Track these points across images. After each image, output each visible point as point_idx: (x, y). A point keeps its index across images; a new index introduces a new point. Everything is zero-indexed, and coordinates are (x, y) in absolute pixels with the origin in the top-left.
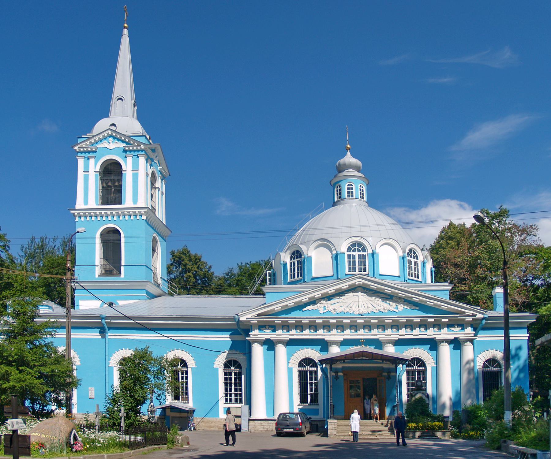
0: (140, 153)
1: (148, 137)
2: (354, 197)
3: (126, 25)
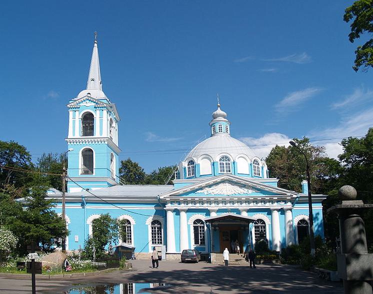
1: (108, 100)
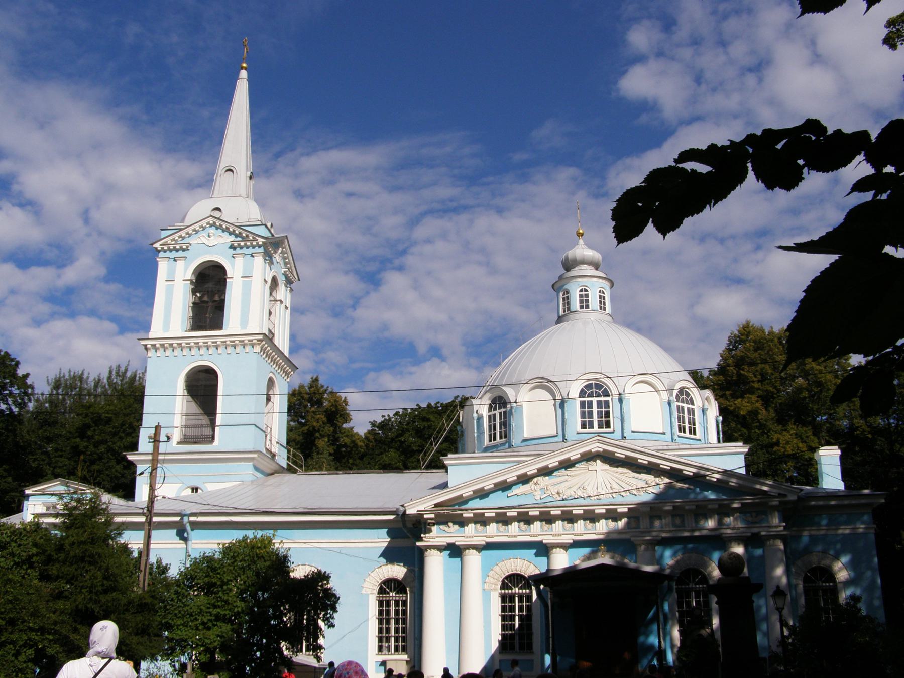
0: (257, 250)
1: (269, 225)
3: (244, 65)
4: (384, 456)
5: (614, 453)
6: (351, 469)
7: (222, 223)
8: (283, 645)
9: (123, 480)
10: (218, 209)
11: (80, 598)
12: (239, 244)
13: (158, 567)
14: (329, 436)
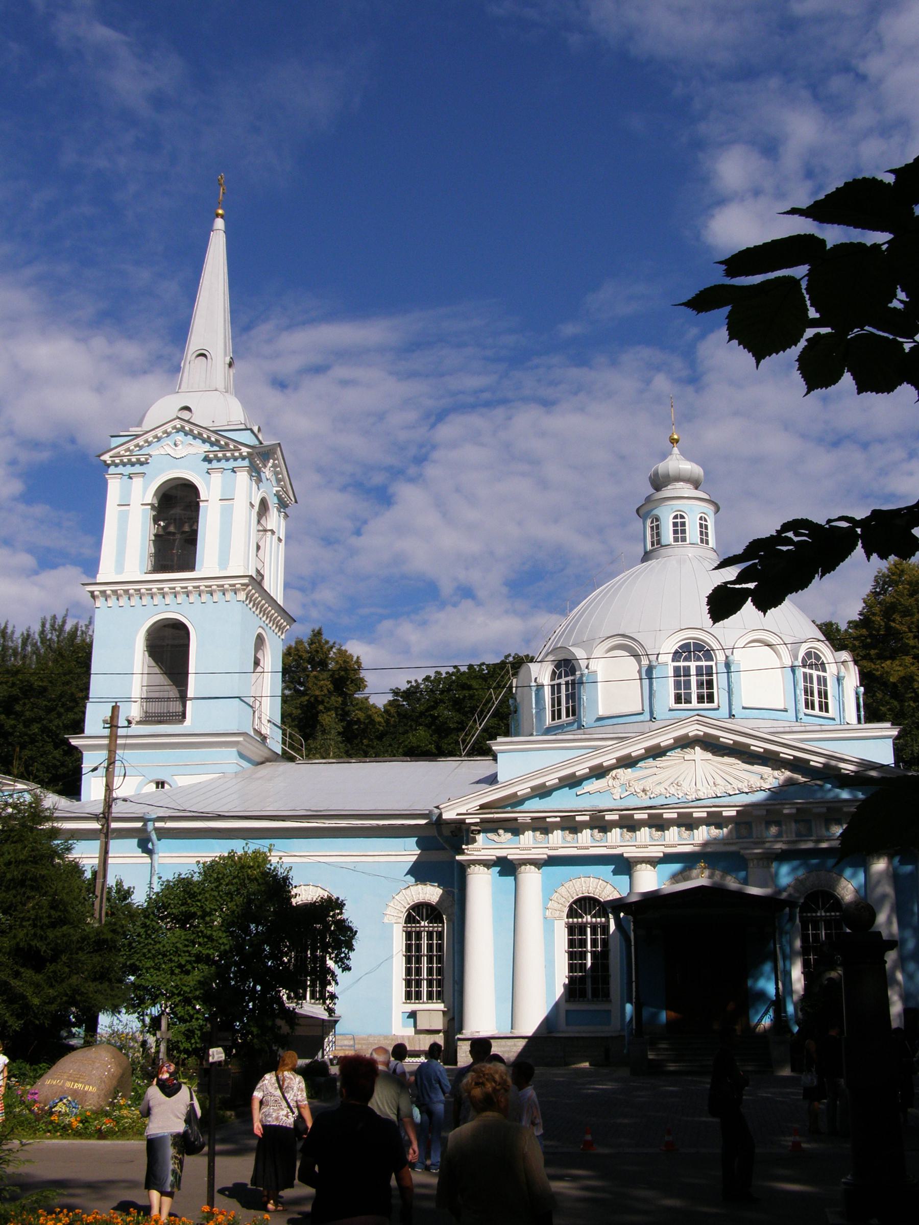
0: (240, 463)
1: (256, 429)
2: (688, 542)
3: (220, 212)
4: (410, 735)
5: (719, 737)
6: (366, 755)
7: (192, 427)
8: (284, 994)
9: (62, 770)
10: (187, 409)
11: (21, 934)
12: (216, 456)
13: (118, 891)
14: (336, 708)
